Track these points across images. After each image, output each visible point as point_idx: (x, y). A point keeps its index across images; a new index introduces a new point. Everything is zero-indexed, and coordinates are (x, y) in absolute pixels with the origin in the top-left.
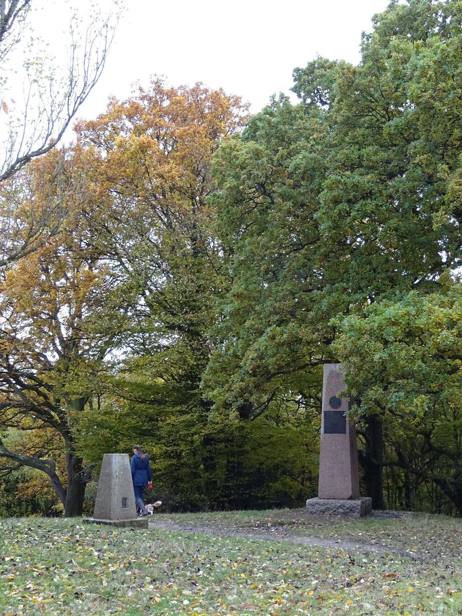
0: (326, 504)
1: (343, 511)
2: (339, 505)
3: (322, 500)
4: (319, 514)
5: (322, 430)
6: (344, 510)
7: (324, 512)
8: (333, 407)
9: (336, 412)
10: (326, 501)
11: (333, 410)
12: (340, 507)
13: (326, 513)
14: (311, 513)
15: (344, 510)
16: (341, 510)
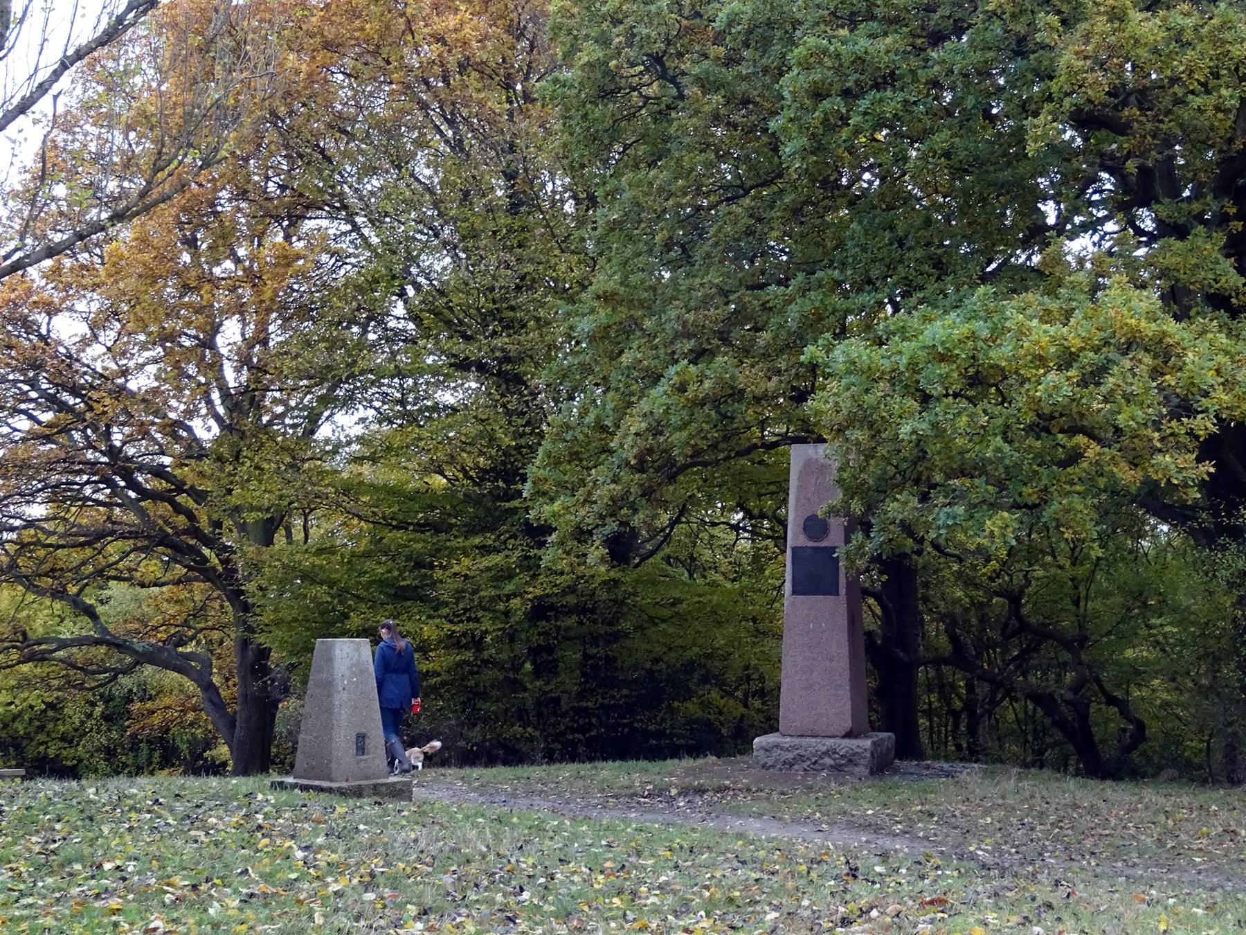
0: (795, 747)
1: (832, 762)
2: (825, 748)
3: (788, 739)
4: (781, 770)
5: (788, 587)
6: (835, 759)
7: (792, 765)
8: (811, 538)
9: (818, 548)
10: (797, 741)
11: (811, 544)
12: (826, 753)
13: (796, 767)
14: (763, 767)
15: (835, 759)
16: (828, 761)
